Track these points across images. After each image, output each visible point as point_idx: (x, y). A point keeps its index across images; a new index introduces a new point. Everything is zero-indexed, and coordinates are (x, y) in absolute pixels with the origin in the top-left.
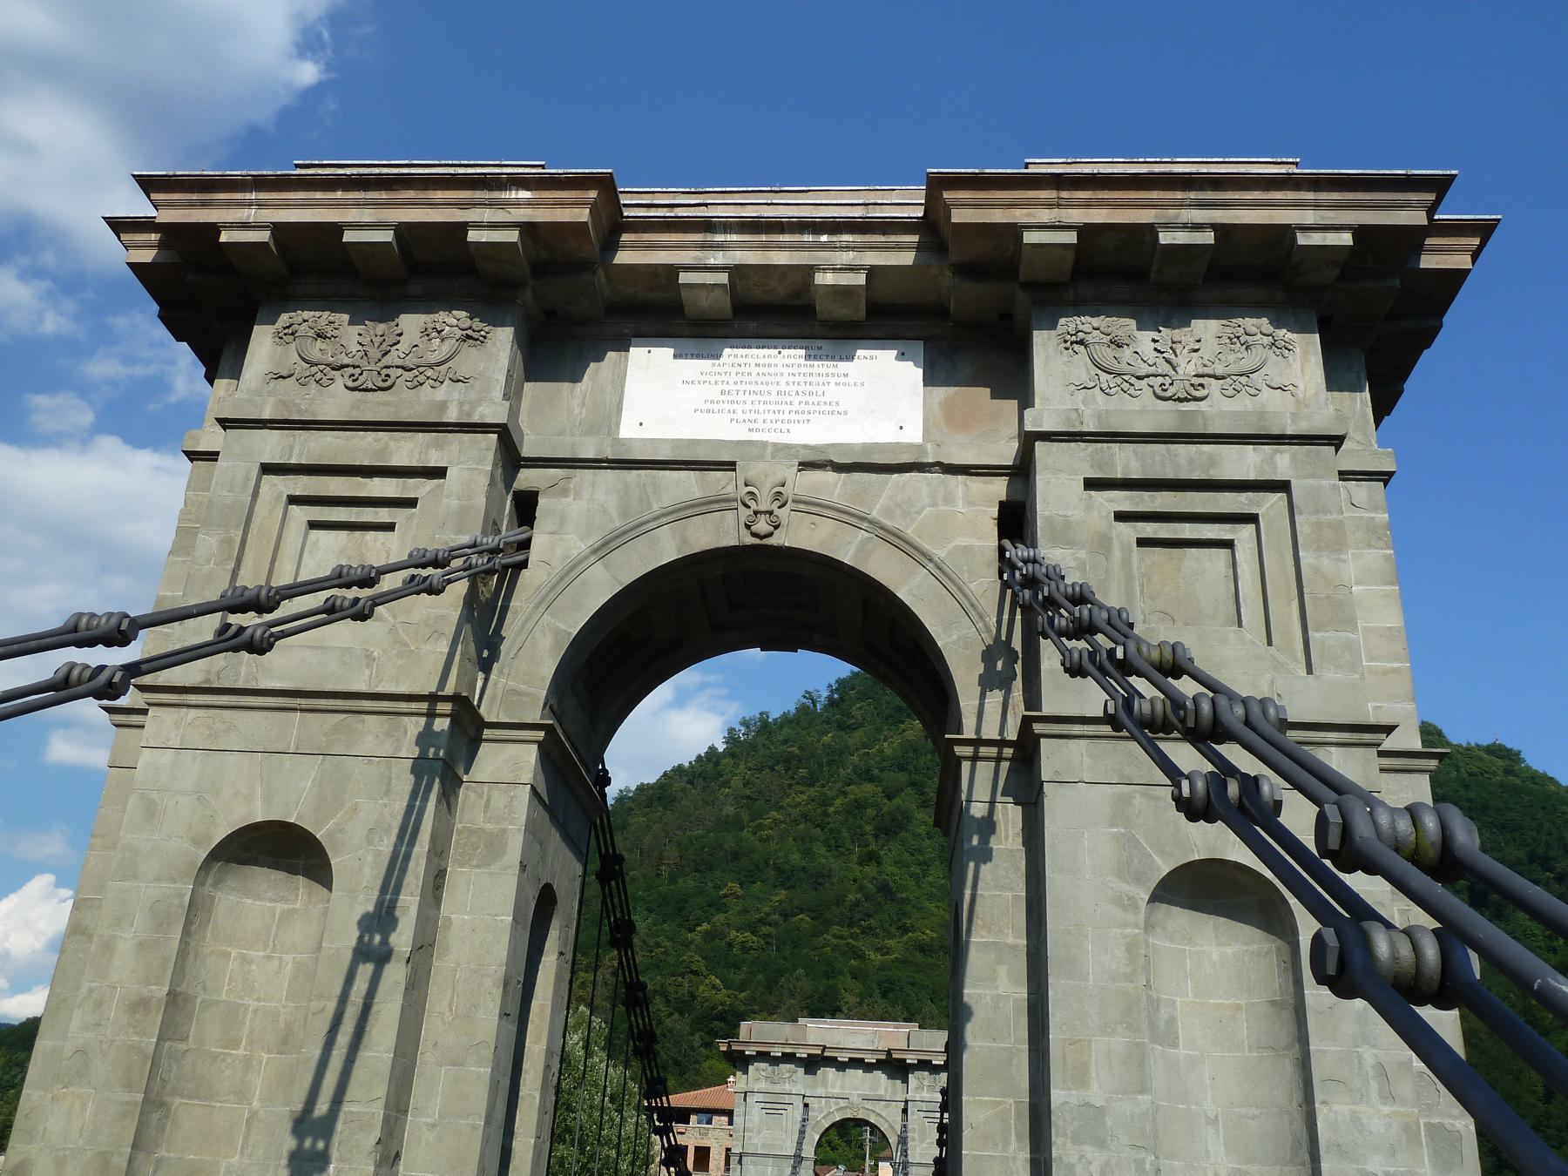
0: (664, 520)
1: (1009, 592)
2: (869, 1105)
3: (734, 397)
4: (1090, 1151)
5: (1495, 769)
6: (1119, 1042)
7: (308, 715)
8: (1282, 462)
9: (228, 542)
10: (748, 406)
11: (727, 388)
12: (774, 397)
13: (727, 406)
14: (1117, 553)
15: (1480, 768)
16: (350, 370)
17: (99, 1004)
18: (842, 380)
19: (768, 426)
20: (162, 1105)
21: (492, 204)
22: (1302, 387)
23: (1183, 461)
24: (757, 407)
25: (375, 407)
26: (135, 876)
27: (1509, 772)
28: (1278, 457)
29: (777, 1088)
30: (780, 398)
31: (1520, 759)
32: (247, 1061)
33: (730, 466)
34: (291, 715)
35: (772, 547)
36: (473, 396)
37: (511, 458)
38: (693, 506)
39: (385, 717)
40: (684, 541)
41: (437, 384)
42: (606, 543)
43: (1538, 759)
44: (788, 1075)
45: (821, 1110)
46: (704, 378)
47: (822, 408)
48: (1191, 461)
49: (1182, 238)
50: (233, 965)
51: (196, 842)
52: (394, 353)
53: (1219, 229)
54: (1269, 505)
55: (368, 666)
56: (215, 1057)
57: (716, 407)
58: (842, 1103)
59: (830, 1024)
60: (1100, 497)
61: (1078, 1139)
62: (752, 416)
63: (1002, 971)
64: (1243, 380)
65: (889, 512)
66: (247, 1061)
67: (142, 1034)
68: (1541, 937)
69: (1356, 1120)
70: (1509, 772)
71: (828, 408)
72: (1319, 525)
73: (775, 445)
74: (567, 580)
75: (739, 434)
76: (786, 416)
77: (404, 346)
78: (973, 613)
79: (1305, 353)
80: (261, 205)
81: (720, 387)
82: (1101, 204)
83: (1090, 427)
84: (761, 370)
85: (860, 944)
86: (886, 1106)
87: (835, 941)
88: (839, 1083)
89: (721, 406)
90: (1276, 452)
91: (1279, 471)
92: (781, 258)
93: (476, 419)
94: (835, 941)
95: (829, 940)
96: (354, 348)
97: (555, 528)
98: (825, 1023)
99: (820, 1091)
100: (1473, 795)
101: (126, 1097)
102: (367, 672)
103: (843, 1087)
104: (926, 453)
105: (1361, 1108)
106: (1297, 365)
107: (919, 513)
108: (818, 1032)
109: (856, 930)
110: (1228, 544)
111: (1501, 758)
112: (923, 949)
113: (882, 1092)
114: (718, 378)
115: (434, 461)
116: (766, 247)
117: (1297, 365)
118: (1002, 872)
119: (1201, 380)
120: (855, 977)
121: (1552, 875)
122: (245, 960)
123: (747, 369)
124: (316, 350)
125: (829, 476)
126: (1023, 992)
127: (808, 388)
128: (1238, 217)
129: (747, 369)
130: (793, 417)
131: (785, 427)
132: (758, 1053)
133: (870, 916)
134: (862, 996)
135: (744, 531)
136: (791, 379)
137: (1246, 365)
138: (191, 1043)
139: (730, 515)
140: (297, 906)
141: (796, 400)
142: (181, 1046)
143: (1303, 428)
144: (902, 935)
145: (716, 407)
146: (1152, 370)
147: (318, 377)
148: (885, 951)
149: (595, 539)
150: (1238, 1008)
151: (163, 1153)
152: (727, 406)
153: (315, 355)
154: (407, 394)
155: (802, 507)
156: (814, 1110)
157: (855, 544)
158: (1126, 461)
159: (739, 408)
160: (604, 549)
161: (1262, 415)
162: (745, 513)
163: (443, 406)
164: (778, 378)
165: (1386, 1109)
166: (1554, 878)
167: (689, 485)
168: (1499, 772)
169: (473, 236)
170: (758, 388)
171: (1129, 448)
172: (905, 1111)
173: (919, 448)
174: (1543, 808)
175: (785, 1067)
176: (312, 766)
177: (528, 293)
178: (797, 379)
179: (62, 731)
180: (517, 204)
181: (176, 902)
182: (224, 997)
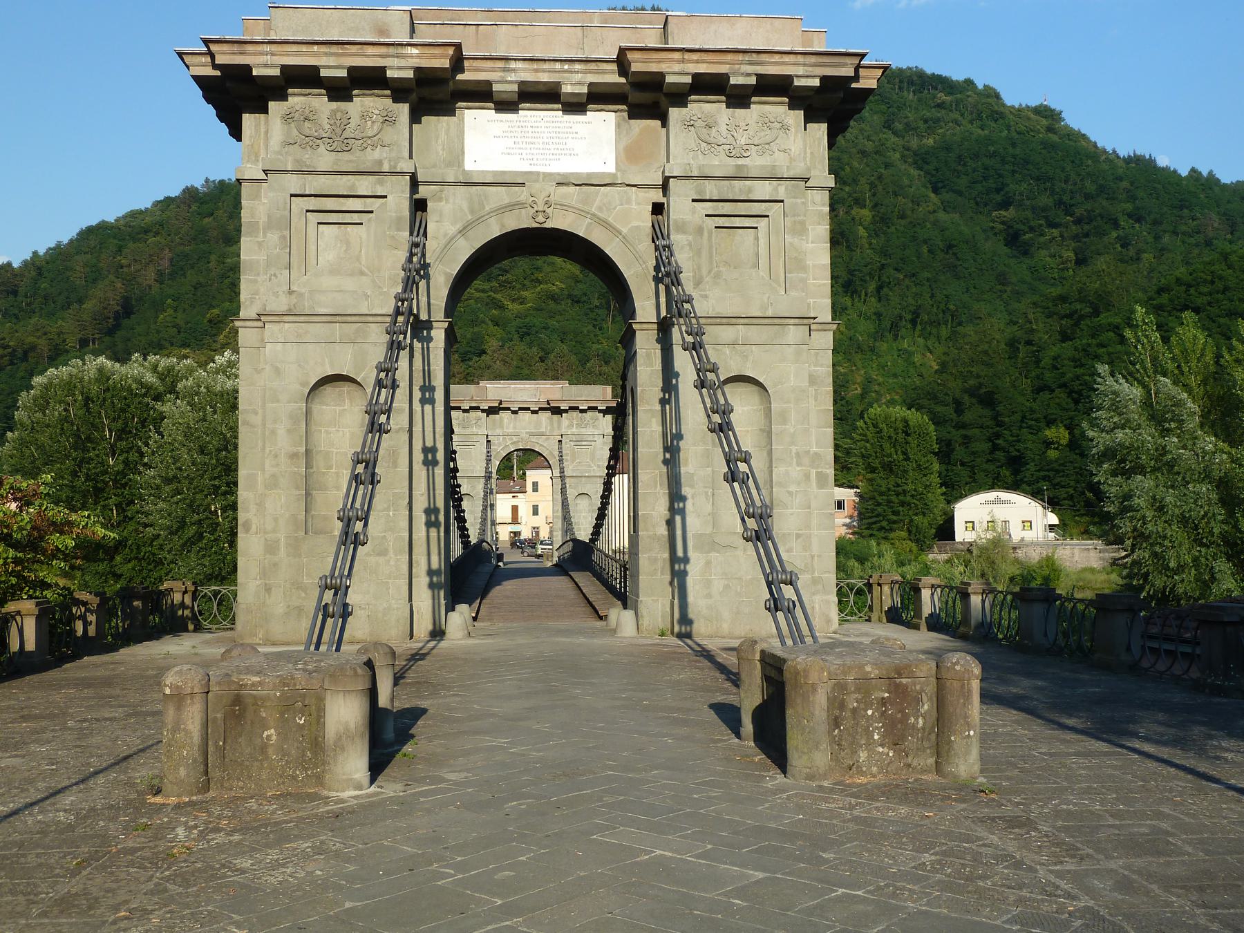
0: (492, 214)
1: (661, 287)
2: (534, 439)
3: (521, 146)
5: (1039, 127)
6: (700, 449)
7: (343, 325)
8: (781, 190)
9: (283, 237)
10: (529, 151)
11: (517, 140)
12: (541, 146)
14: (706, 234)
15: (1026, 126)
17: (276, 456)
18: (575, 135)
19: (539, 162)
20: (310, 494)
21: (398, 56)
22: (793, 150)
23: (737, 190)
24: (533, 151)
25: (346, 161)
26: (278, 401)
27: (1050, 129)
28: (779, 188)
30: (544, 146)
31: (1060, 118)
32: (337, 474)
34: (334, 325)
36: (394, 155)
37: (414, 183)
38: (506, 207)
39: (379, 324)
40: (503, 226)
41: (374, 148)
42: (464, 228)
43: (1074, 119)
44: (474, 422)
45: (500, 444)
46: (505, 134)
47: (566, 152)
48: (740, 190)
50: (323, 435)
52: (348, 130)
53: (759, 76)
55: (367, 299)
56: (324, 473)
57: (512, 151)
58: (515, 439)
59: (503, 384)
62: (531, 157)
63: (654, 420)
64: (767, 146)
65: (600, 209)
66: (337, 474)
67: (298, 467)
68: (1056, 270)
70: (1050, 129)
71: (568, 152)
73: (544, 173)
74: (448, 247)
75: (525, 167)
76: (548, 157)
77: (352, 125)
78: (640, 261)
79: (796, 132)
80: (273, 54)
81: (514, 140)
82: (703, 61)
84: (534, 130)
85: (498, 296)
86: (547, 439)
87: (478, 295)
88: (512, 425)
89: (515, 151)
90: (779, 185)
91: (780, 195)
92: (544, 77)
94: (478, 295)
95: (472, 294)
97: (438, 219)
98: (497, 384)
99: (498, 431)
100: (1018, 151)
101: (298, 493)
102: (366, 303)
103: (515, 428)
104: (617, 178)
105: (790, 468)
107: (615, 209)
109: (494, 284)
111: (1045, 117)
112: (553, 298)
114: (512, 134)
116: (536, 71)
118: (653, 379)
119: (747, 147)
120: (496, 324)
121: (1072, 219)
122: (328, 433)
123: (526, 129)
125: (572, 189)
126: (660, 429)
127: (558, 141)
128: (767, 70)
129: (526, 129)
130: (552, 157)
133: (507, 272)
134: (503, 341)
136: (549, 135)
137: (768, 139)
138: (314, 469)
140: (346, 408)
141: (552, 147)
142: (312, 471)
143: (791, 174)
144: (535, 287)
145: (512, 151)
146: (724, 141)
147: (311, 143)
148: (523, 301)
149: (459, 226)
150: (748, 431)
151: (313, 513)
153: (307, 132)
154: (358, 153)
155: (559, 207)
156: (494, 444)
157: (585, 226)
158: (711, 189)
159: (524, 152)
160: (463, 231)
163: (380, 162)
164: (542, 135)
165: (799, 468)
166: (1072, 222)
168: (1042, 130)
170: (533, 140)
173: (614, 175)
174: (1073, 162)
177: (415, 94)
178: (552, 135)
179: (1161, 716)
180: (411, 56)
181: (300, 412)
182: (323, 449)
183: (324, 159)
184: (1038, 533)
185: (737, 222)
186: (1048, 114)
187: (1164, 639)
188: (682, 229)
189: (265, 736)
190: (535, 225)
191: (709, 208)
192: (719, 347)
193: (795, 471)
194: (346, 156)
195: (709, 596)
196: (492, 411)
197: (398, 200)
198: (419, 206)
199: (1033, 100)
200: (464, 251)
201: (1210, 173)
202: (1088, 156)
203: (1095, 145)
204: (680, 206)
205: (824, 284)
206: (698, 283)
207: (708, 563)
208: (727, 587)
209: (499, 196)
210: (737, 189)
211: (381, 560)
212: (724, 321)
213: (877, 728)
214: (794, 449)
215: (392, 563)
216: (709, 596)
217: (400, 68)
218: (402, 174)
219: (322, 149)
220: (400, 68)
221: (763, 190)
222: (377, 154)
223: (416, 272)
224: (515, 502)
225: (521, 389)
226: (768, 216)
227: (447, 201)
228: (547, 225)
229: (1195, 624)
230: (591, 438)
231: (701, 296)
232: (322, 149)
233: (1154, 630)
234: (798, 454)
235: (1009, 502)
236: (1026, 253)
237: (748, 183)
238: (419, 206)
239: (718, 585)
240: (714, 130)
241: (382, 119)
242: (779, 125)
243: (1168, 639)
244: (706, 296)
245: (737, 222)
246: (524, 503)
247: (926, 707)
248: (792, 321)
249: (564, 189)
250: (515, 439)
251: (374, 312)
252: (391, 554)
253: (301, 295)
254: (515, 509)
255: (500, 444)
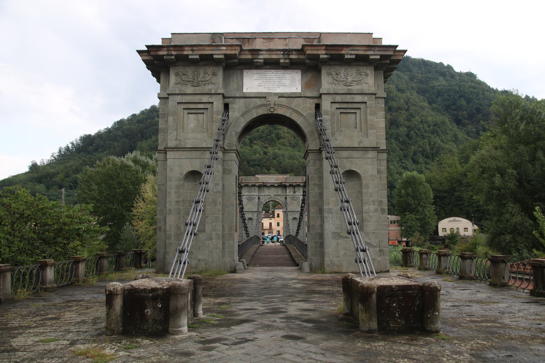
2: (276, 197)
4: (330, 215)
8: (366, 98)
13: (263, 85)
14: (336, 116)
16: (191, 82)
17: (170, 202)
25: (198, 90)
29: (251, 194)
33: (265, 97)
35: (275, 114)
42: (243, 114)
43: (481, 77)
45: (263, 199)
49: (349, 57)
51: (181, 174)
54: (362, 106)
58: (269, 197)
60: (333, 105)
61: (328, 213)
65: (295, 106)
69: (369, 208)
72: (371, 111)
83: (332, 92)
92: (274, 57)
93: (218, 92)
96: (191, 77)
99: (263, 194)
106: (370, 78)
108: (262, 178)
110: (356, 113)
113: (279, 193)
115: (211, 101)
116: (270, 54)
117: (370, 78)
124: (184, 78)
125: (284, 99)
130: (276, 87)
131: (275, 89)
132: (245, 185)
135: (268, 111)
139: (266, 107)
141: (277, 83)
143: (369, 92)
146: (343, 80)
149: (241, 114)
152: (263, 85)
153: (184, 79)
154: (203, 87)
158: (338, 98)
159: (266, 85)
160: (243, 115)
161: (362, 89)
162: (268, 107)
163: (211, 90)
167: (258, 102)
169: (215, 57)
171: (339, 96)
172: (286, 198)
175: (253, 188)
176: (198, 161)
180: (223, 50)
183: (190, 89)
184: (470, 233)
185: (349, 111)
186: (471, 75)
187: (518, 273)
188: (327, 114)
189: (146, 311)
190: (270, 113)
191: (338, 106)
192: (341, 159)
193: (372, 207)
194: (198, 88)
195: (338, 257)
196: (260, 187)
197: (218, 104)
198: (226, 107)
199: (465, 70)
200: (243, 123)
201: (533, 97)
202: (487, 91)
203: (489, 87)
204: (326, 104)
205: (383, 135)
206: (333, 135)
207: (338, 244)
208: (345, 253)
209: (258, 102)
210: (348, 98)
211: (210, 242)
212: (344, 149)
213: (398, 311)
214: (371, 199)
215: (214, 243)
216: (338, 257)
217: (218, 54)
218: (219, 94)
219: (189, 86)
220: (218, 54)
221: (358, 98)
222: (210, 87)
223: (223, 131)
224: (271, 221)
225: (271, 178)
226: (360, 108)
227: (236, 104)
228: (275, 112)
229: (531, 267)
230: (298, 197)
231: (335, 139)
232: (189, 86)
233: (515, 270)
234: (373, 201)
235: (459, 221)
236: (464, 126)
237: (353, 96)
238: (226, 107)
239: (342, 253)
240: (339, 76)
241: (212, 74)
242: (364, 74)
243: (520, 273)
244: (336, 139)
245: (349, 111)
246: (274, 222)
247: (418, 303)
248: (370, 149)
249: (281, 99)
250: (269, 197)
251: (208, 147)
252: (214, 240)
253: (180, 140)
254: (271, 224)
255: (263, 199)
